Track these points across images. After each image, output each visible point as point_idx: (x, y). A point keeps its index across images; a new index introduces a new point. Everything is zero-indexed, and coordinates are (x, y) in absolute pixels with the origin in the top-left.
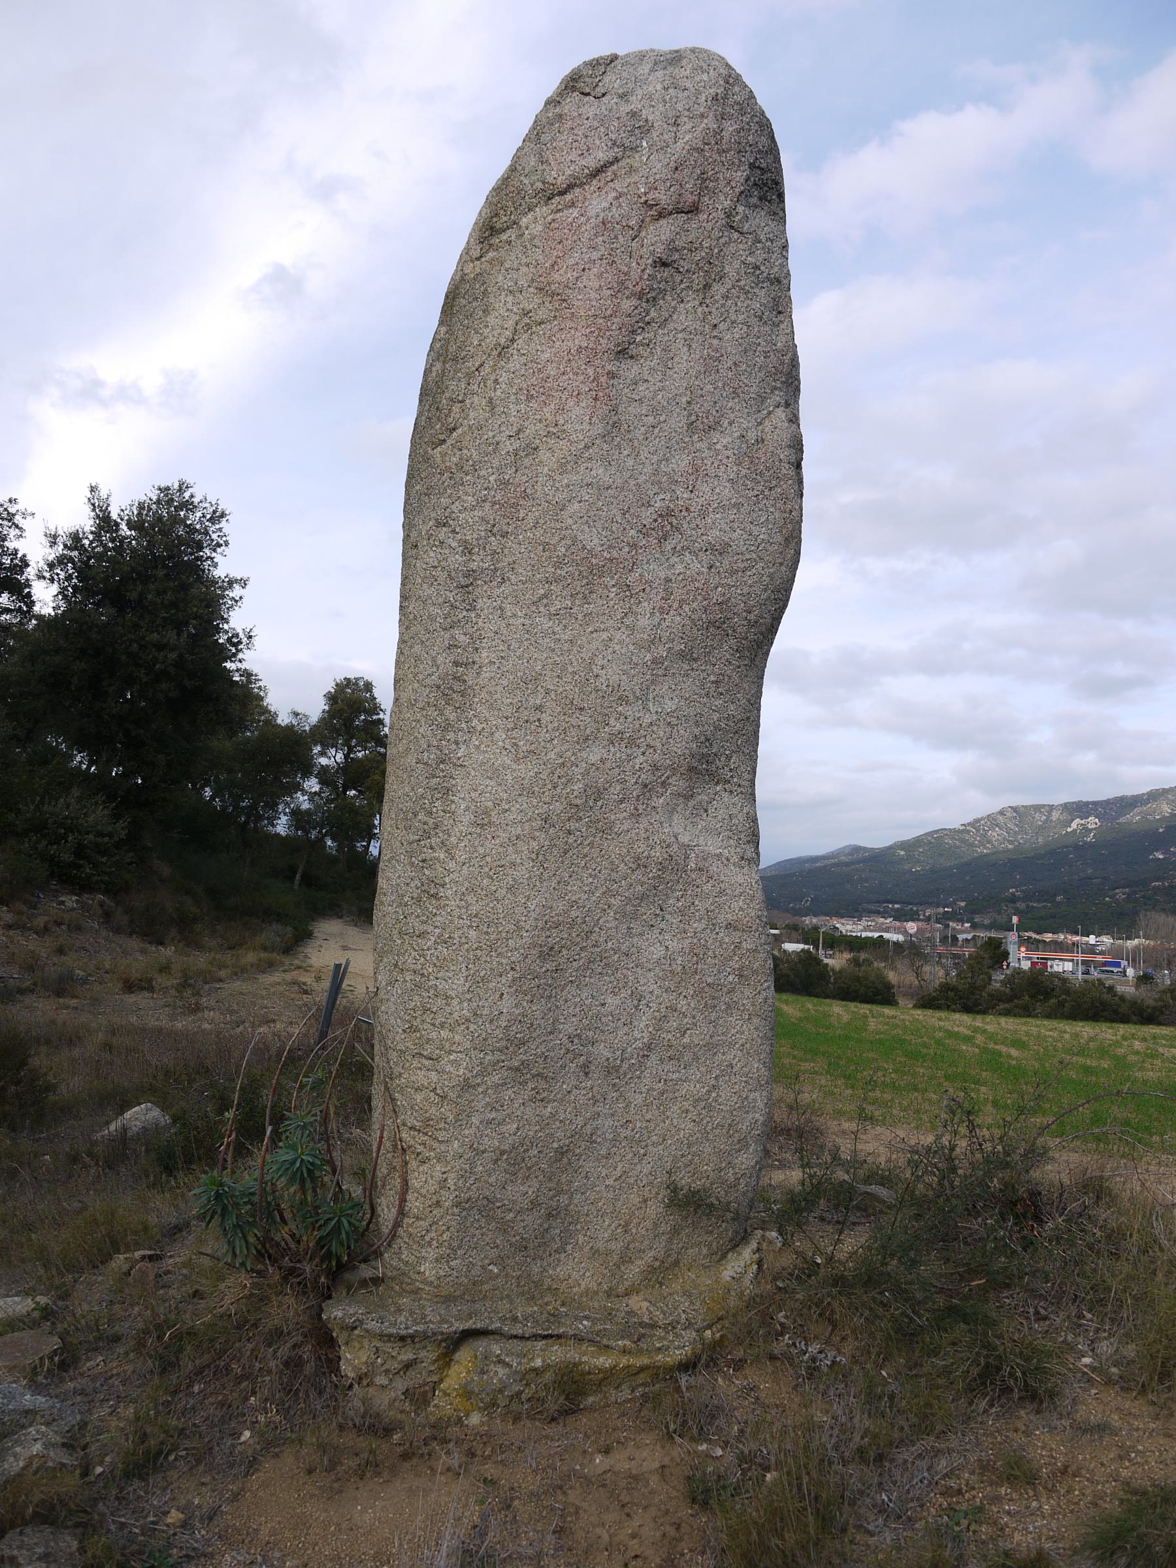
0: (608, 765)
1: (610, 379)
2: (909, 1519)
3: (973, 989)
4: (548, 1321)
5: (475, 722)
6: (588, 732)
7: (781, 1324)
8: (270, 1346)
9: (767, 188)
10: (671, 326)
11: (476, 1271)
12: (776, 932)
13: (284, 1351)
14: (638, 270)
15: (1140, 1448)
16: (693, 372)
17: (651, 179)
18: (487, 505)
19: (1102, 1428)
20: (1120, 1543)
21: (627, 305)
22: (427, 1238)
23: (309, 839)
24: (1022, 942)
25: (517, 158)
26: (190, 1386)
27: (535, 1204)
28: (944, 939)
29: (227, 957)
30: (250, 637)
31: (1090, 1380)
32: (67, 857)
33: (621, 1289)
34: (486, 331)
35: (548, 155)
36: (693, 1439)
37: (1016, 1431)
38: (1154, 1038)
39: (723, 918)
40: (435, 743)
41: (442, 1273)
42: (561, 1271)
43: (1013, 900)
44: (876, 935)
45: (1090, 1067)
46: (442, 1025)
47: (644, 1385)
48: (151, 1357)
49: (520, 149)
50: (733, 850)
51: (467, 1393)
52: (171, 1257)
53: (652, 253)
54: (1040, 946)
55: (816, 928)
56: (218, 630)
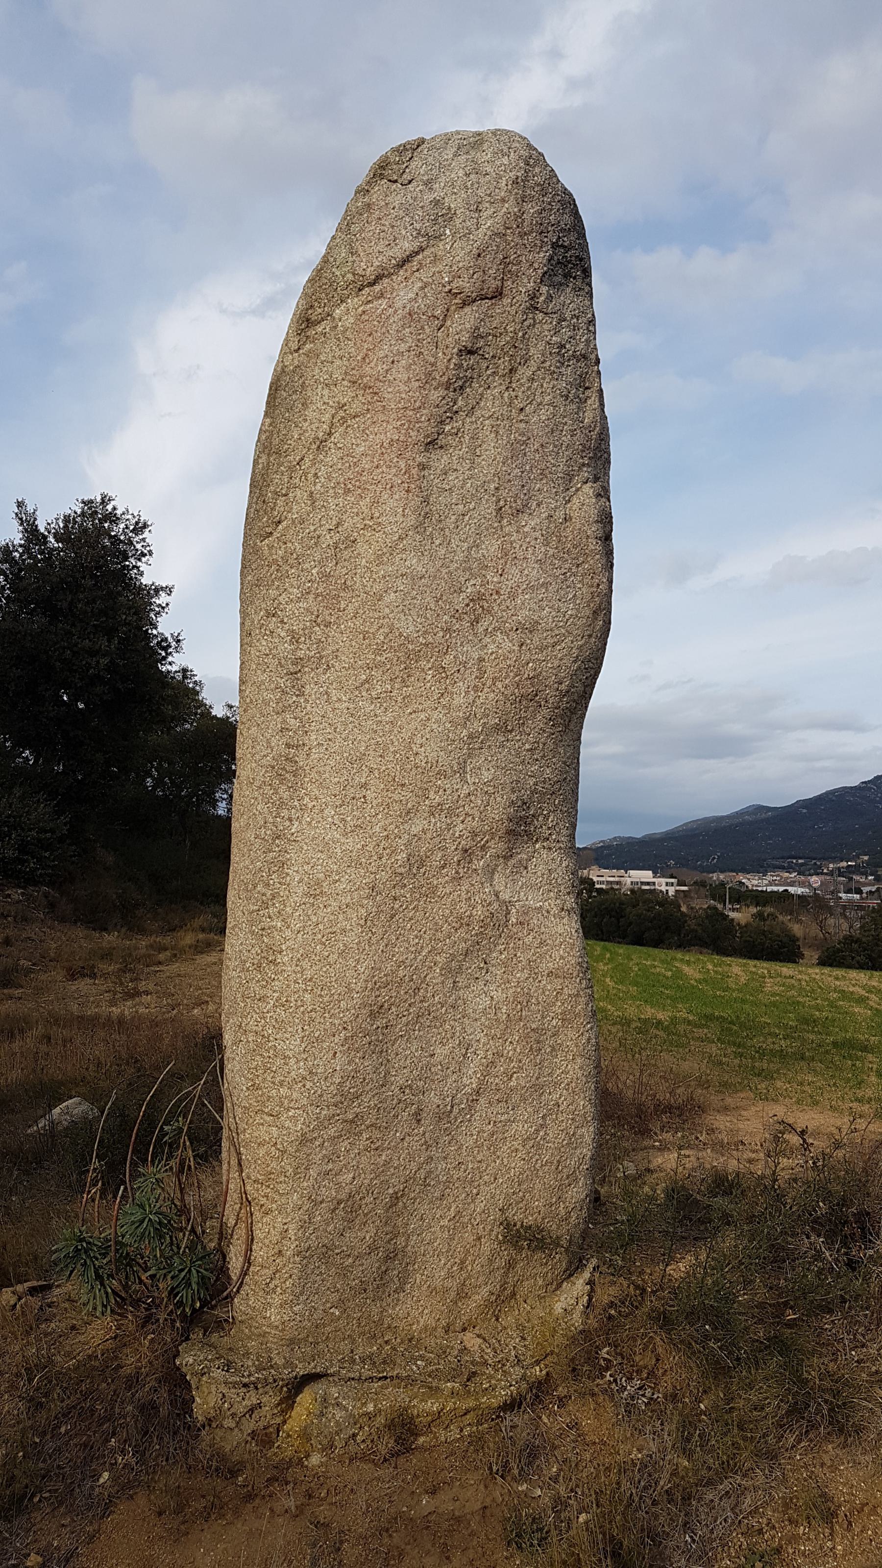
1: (421, 470)
5: (307, 799)
6: (409, 805)
9: (570, 264)
10: (478, 413)
14: (444, 361)
17: (455, 268)
21: (435, 395)
22: (272, 1286)
27: (373, 1249)
29: (167, 940)
30: (178, 641)
32: (10, 853)
33: (458, 1326)
36: (514, 1479)
37: (822, 1465)
39: (546, 966)
41: (286, 1318)
44: (781, 889)
46: (281, 1084)
50: (552, 902)
51: (305, 1435)
52: (58, 1286)
55: (722, 884)
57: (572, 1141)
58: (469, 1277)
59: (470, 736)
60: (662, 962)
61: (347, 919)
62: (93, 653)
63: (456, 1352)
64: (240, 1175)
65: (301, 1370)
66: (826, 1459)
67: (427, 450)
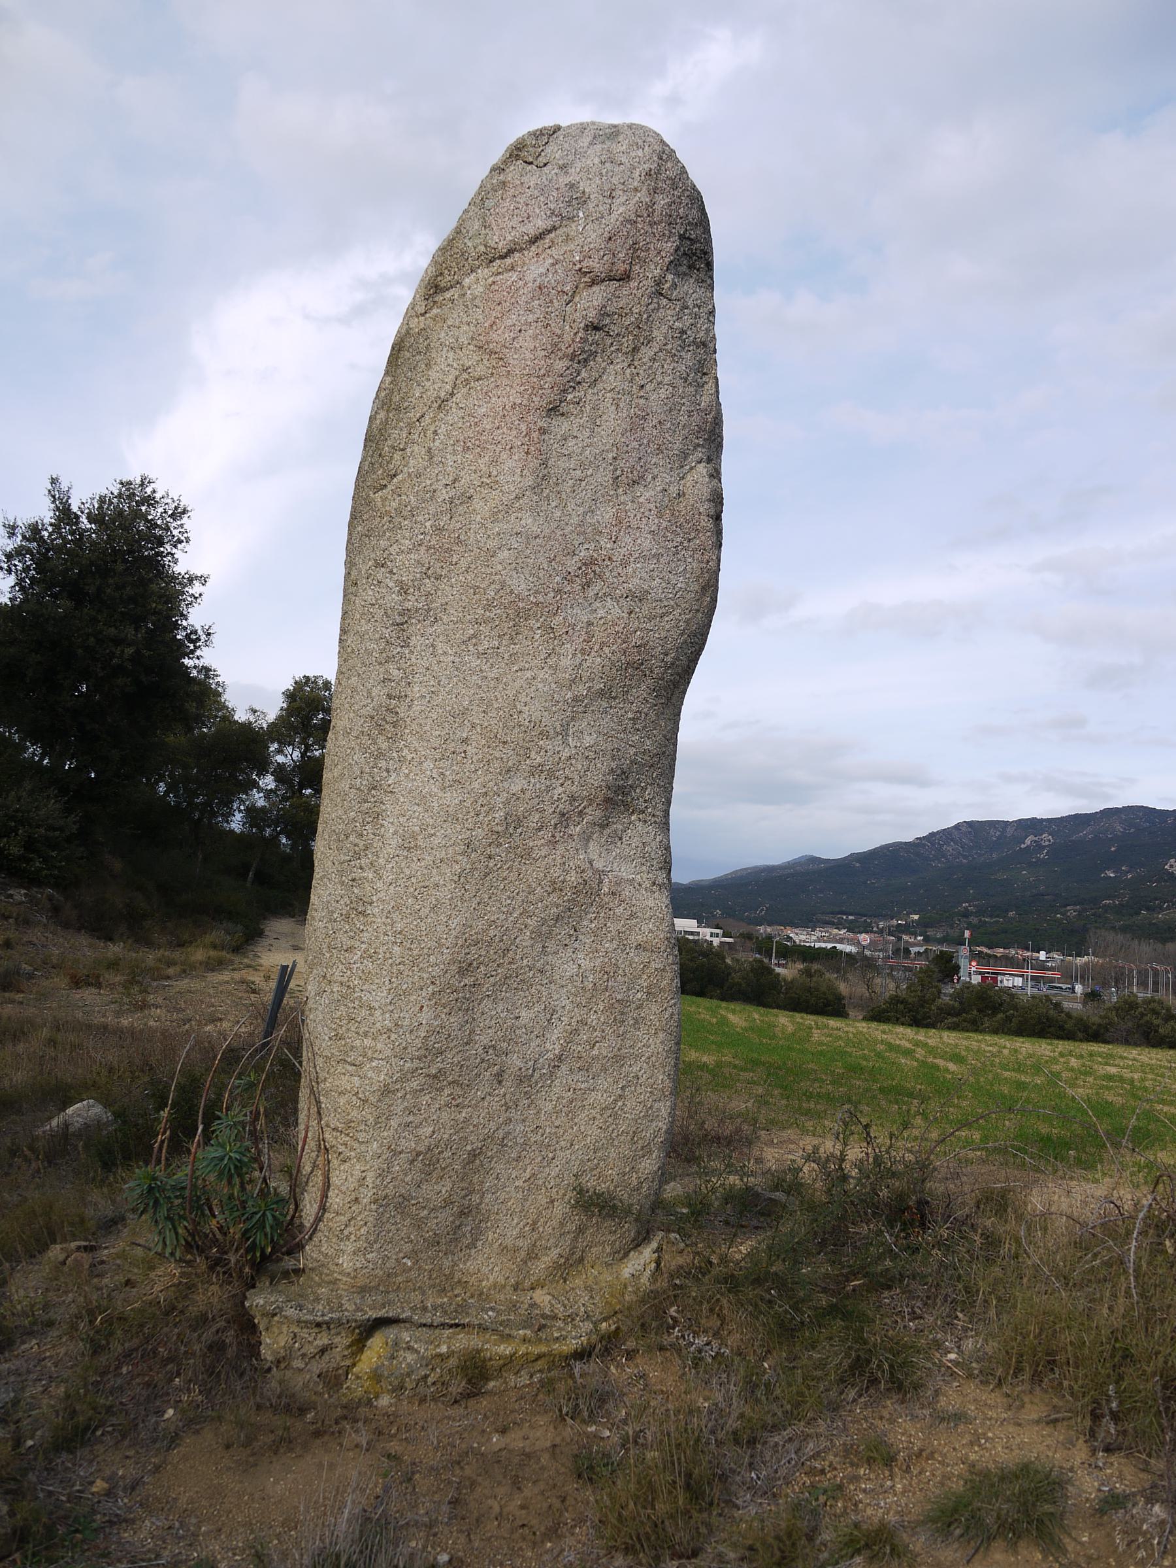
0: (528, 796)
2: (774, 1495)
3: (923, 1002)
4: (456, 1311)
5: (406, 751)
6: (510, 764)
7: (672, 1318)
8: (195, 1331)
9: (695, 255)
10: (600, 386)
11: (391, 1264)
12: (730, 940)
13: (208, 1335)
14: (571, 334)
15: (990, 1435)
16: (619, 430)
17: (586, 248)
18: (423, 549)
19: (959, 1417)
20: (956, 1516)
21: (560, 365)
22: (346, 1232)
23: (264, 837)
24: (973, 956)
25: (462, 221)
26: (118, 1367)
27: (448, 1203)
28: (896, 952)
29: (177, 955)
30: (209, 634)
31: (953, 1374)
32: (15, 850)
33: (527, 1284)
34: (428, 384)
35: (491, 220)
36: (583, 1421)
37: (881, 1418)
38: (1091, 1055)
39: (634, 938)
40: (368, 770)
41: (359, 1265)
42: (471, 1266)
43: (966, 914)
44: (829, 946)
45: (1023, 1083)
46: (366, 1034)
47: (540, 1371)
48: (82, 1340)
49: (466, 211)
50: (645, 876)
51: (376, 1376)
52: (106, 1248)
53: (585, 317)
54: (992, 961)
55: (770, 938)
56: (176, 626)
57: (649, 1115)
58: (540, 1238)
59: (575, 699)
60: (707, 1009)
61: (440, 874)
62: (117, 642)
63: (526, 1306)
64: (319, 1123)
65: (373, 1314)
66: (885, 1414)
67: (548, 416)
